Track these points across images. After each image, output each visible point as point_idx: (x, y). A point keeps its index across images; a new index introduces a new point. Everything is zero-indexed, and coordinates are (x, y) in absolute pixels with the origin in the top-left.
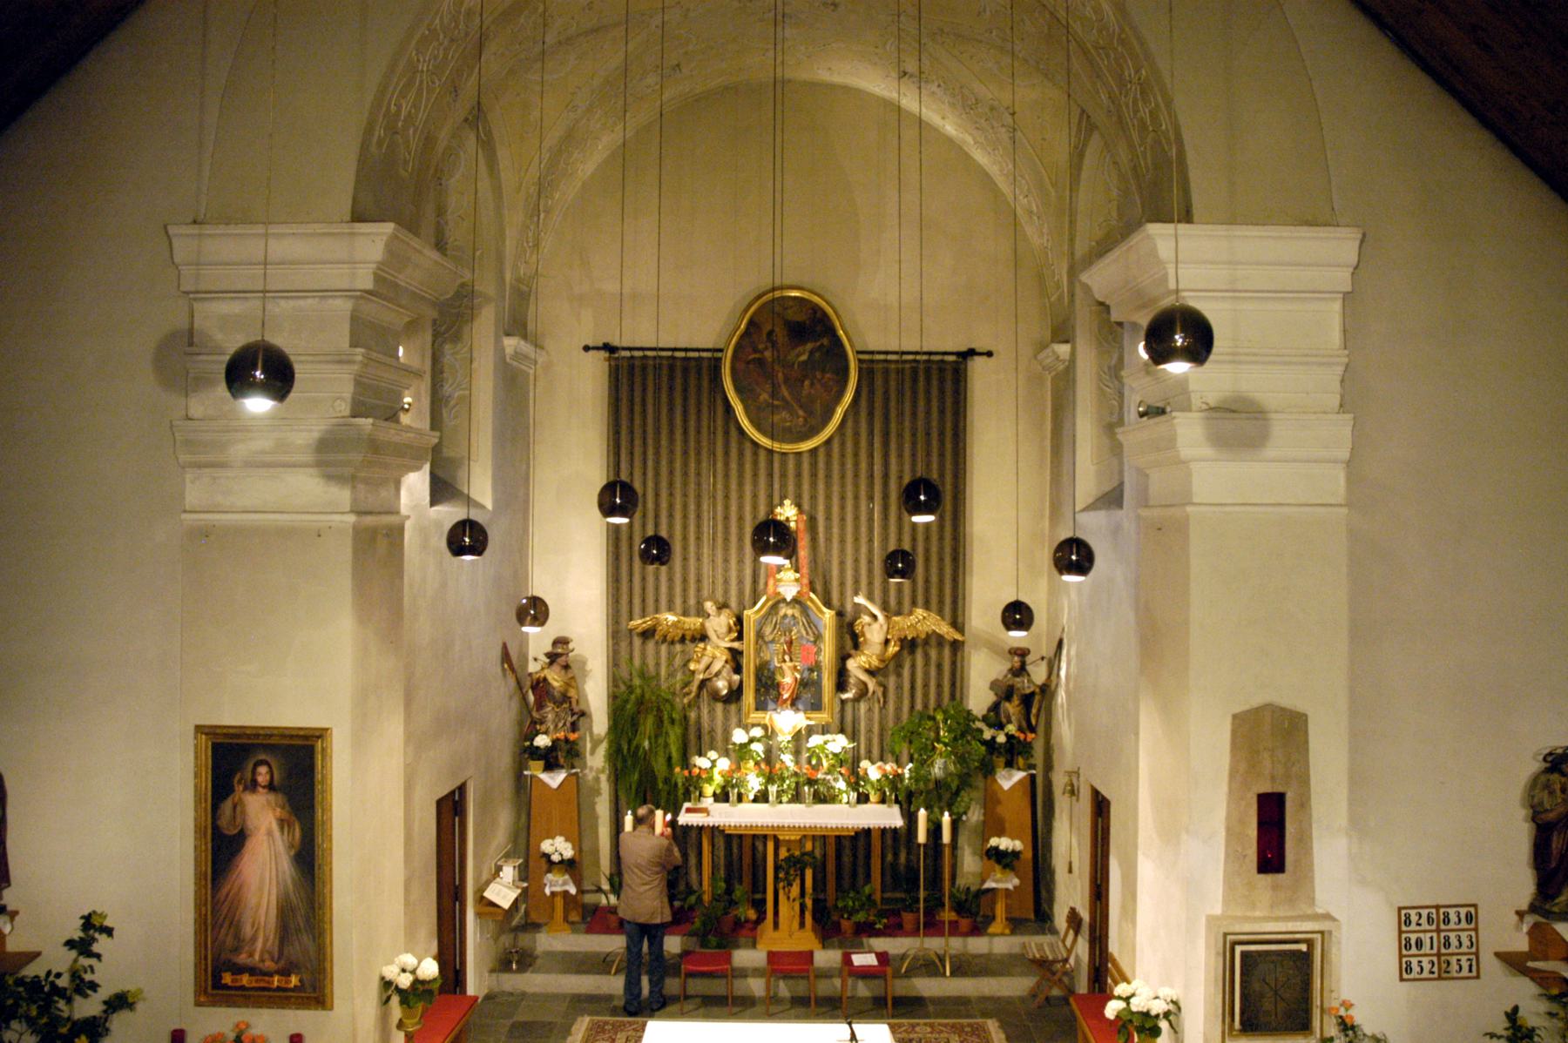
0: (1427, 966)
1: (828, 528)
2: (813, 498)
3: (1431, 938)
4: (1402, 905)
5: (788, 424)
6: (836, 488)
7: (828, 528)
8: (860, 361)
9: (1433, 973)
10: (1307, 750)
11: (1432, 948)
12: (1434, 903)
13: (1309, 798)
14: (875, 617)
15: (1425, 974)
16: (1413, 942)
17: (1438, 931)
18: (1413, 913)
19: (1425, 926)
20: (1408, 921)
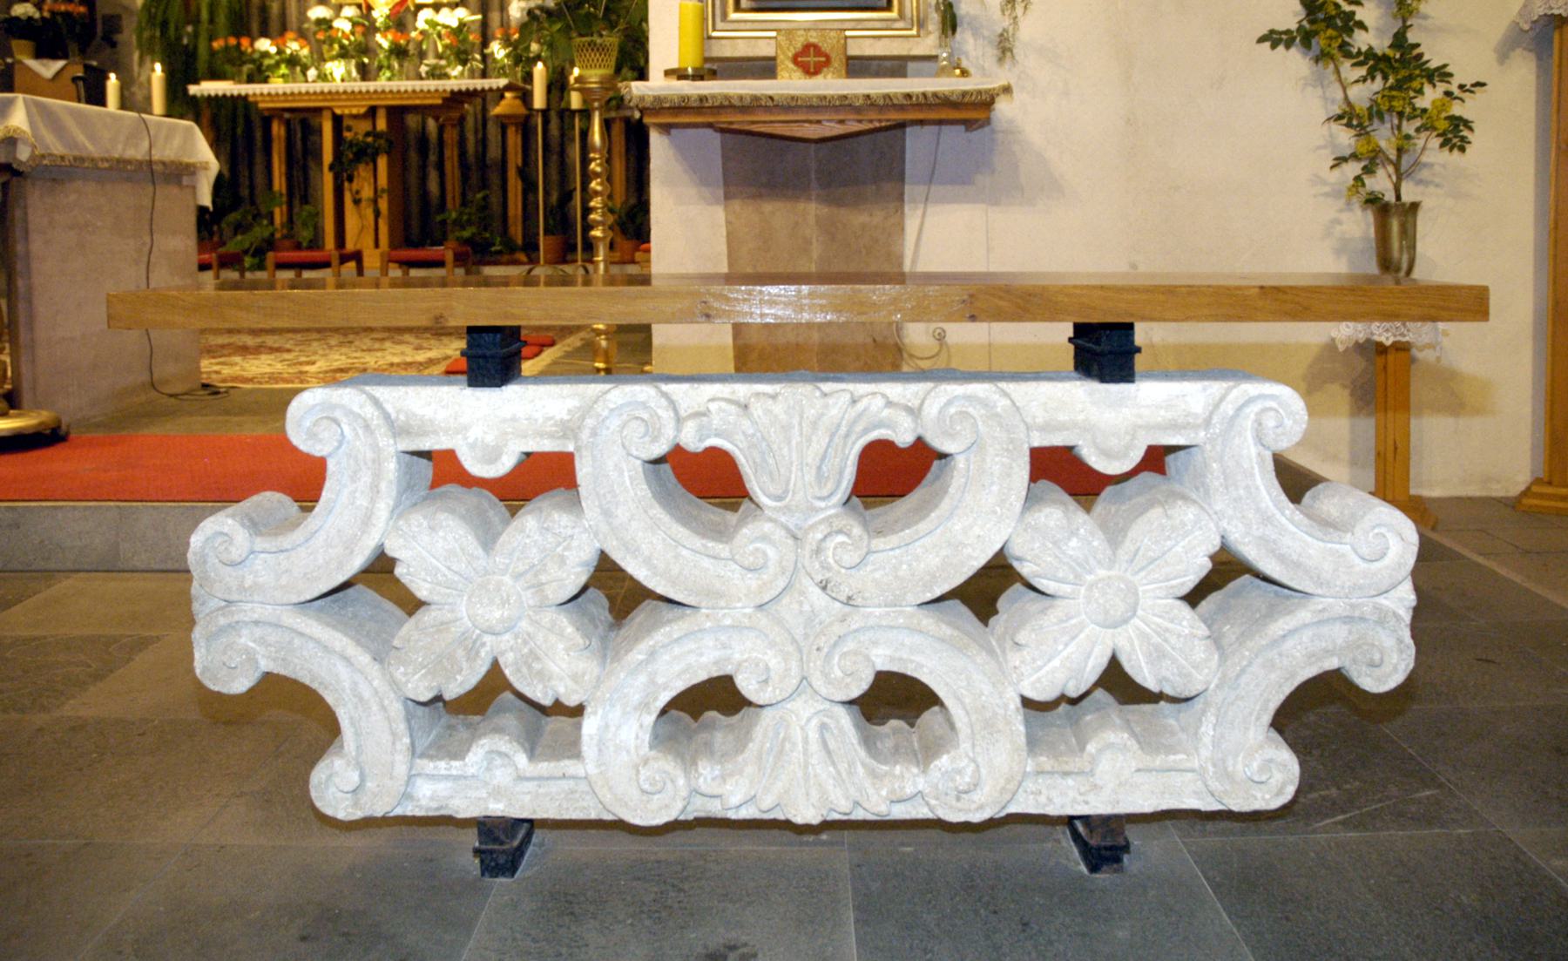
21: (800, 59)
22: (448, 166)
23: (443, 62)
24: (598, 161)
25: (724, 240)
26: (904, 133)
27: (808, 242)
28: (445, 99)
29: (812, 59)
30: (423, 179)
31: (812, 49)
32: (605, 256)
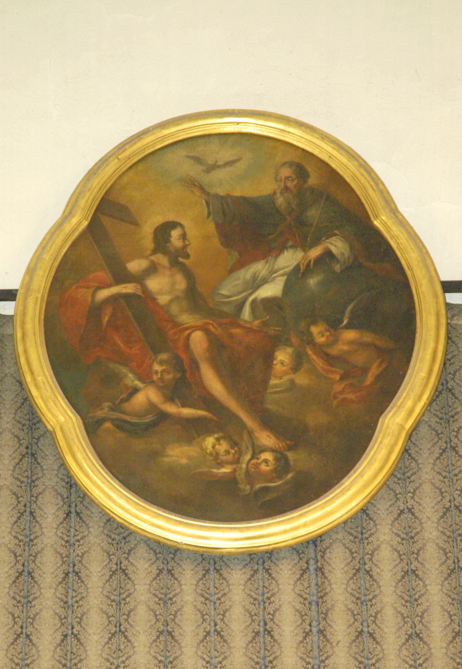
5: (226, 470)
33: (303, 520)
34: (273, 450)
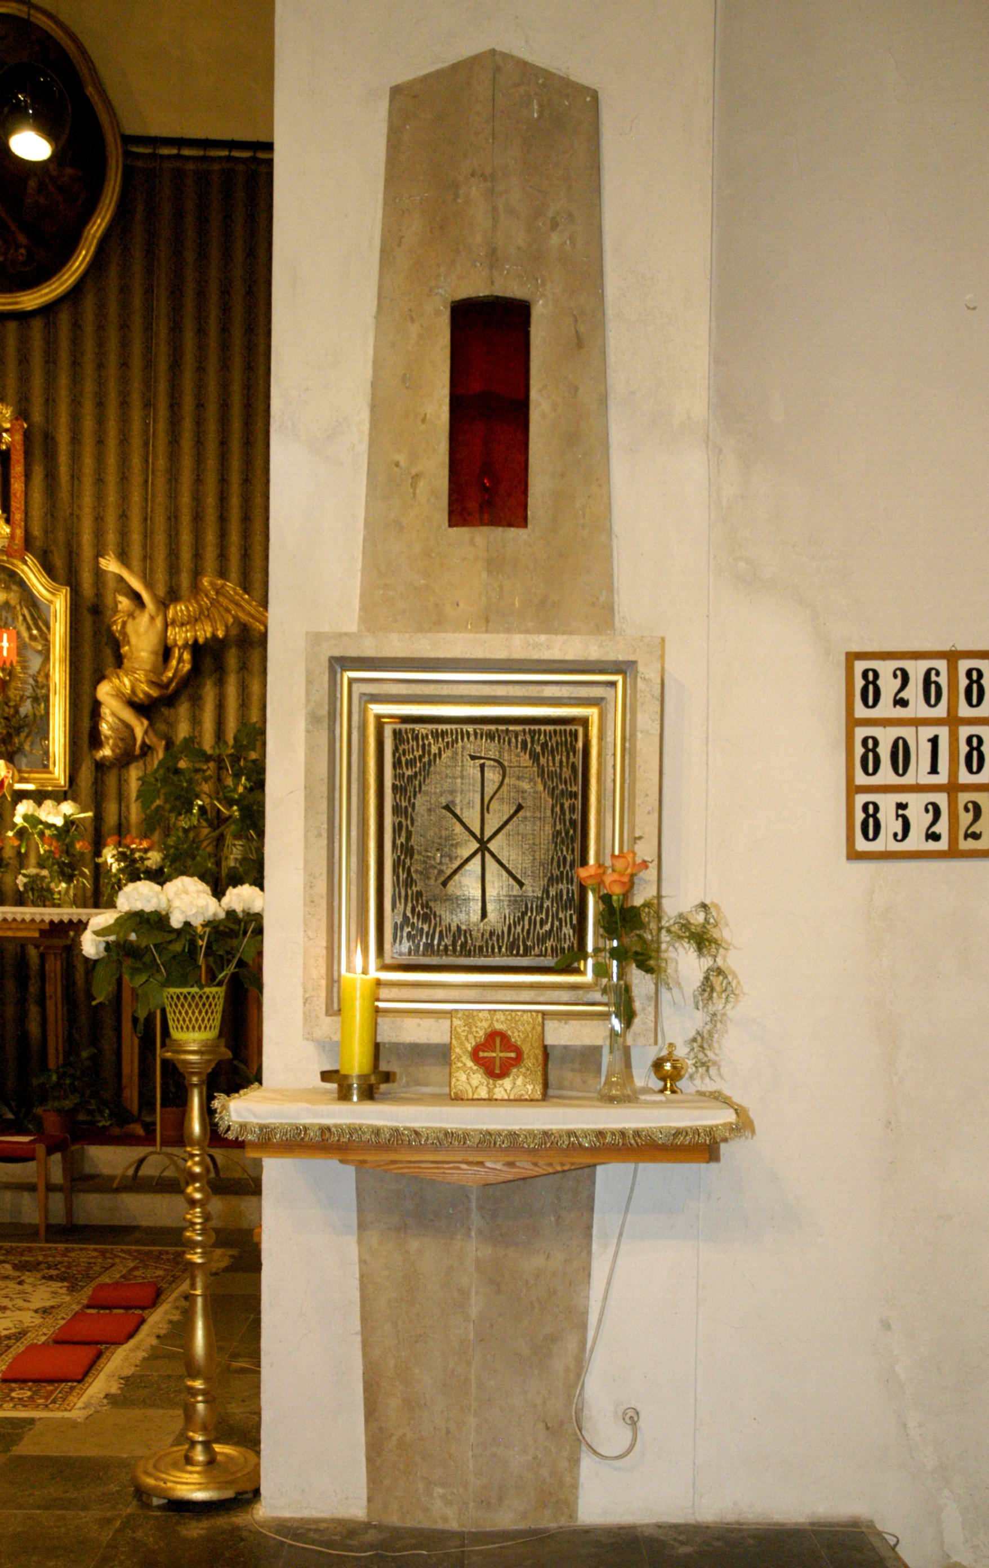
0: (920, 820)
1: (75, 457)
2: (50, 401)
3: (934, 741)
4: (855, 648)
6: (89, 386)
7: (75, 457)
8: (127, 154)
9: (936, 837)
10: (597, 190)
11: (934, 770)
12: (946, 648)
13: (599, 324)
14: (137, 598)
15: (916, 841)
16: (884, 751)
17: (953, 721)
18: (886, 669)
19: (918, 708)
20: (871, 693)
21: (481, 1054)
22: (50, 1005)
23: (45, 873)
24: (197, 1159)
25: (356, 1283)
26: (554, 1046)
27: (464, 1293)
28: (42, 932)
29: (496, 1054)
30: (22, 1018)
31: (498, 1040)
32: (206, 1288)
33: (39, 294)
34: (25, 247)
